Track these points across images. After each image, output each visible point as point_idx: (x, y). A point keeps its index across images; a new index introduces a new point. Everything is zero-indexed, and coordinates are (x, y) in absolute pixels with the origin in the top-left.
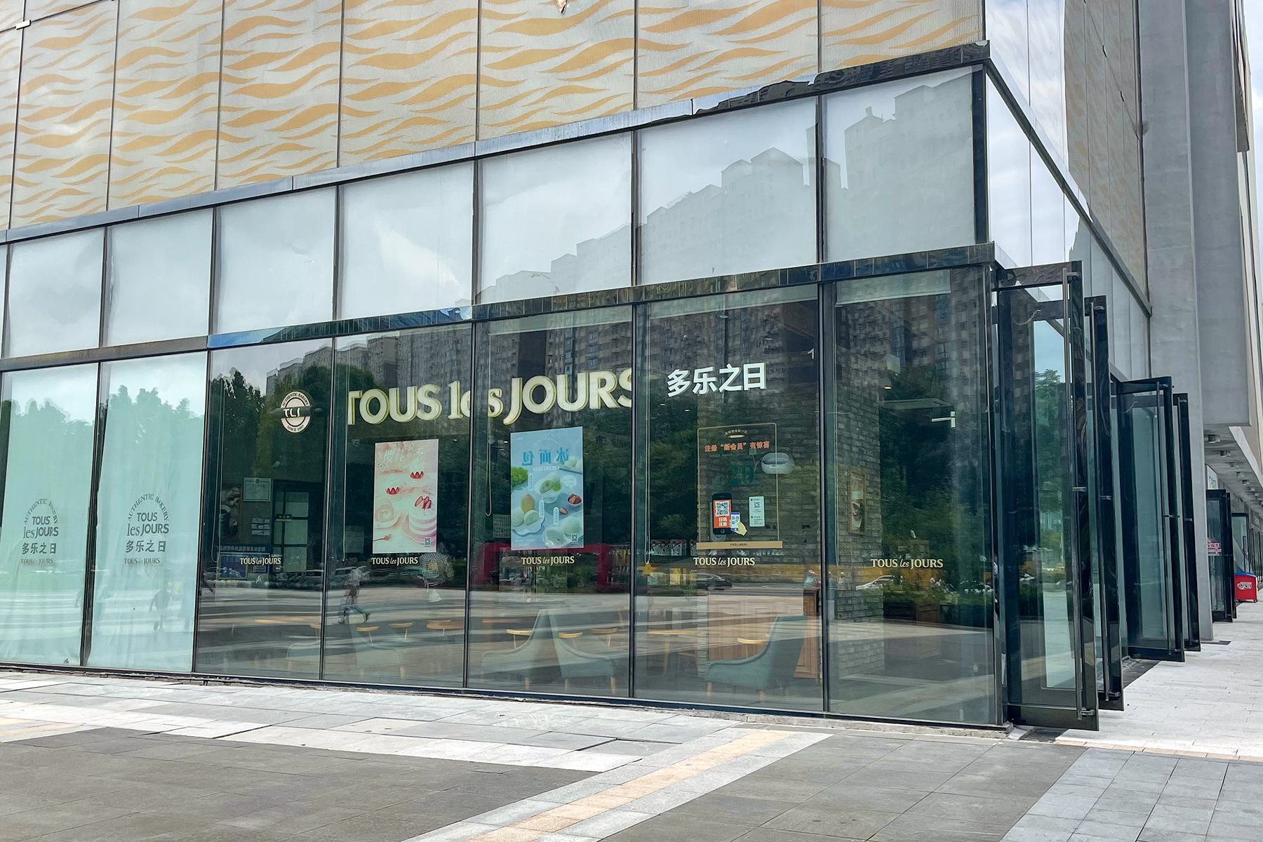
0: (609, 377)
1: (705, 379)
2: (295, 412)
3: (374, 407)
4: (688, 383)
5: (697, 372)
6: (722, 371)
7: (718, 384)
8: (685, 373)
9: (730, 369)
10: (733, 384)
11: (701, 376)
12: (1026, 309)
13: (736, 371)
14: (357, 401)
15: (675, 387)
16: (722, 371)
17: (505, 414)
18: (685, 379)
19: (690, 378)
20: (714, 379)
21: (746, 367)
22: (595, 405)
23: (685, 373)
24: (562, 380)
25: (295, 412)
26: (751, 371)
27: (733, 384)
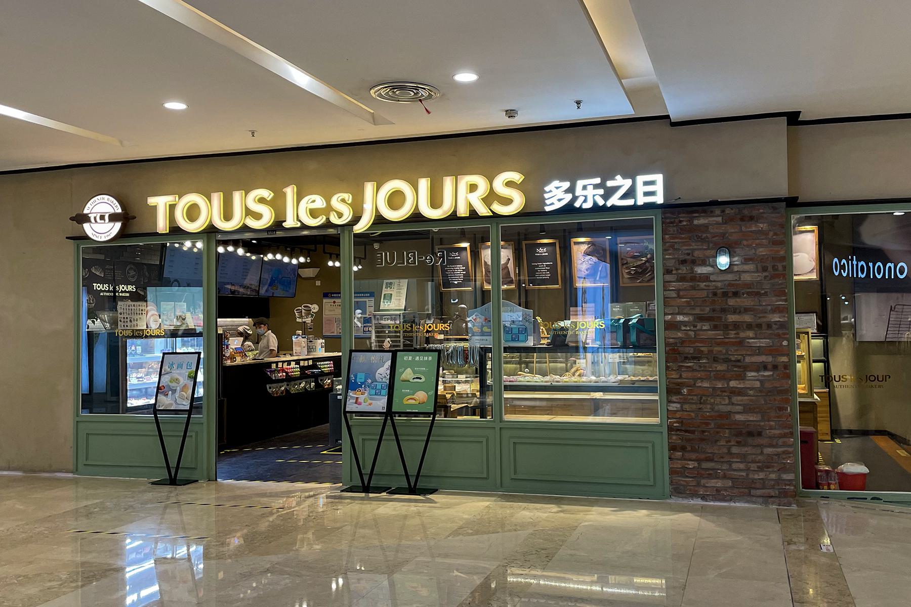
0: (480, 181)
1: (590, 192)
2: (102, 217)
3: (192, 213)
4: (569, 197)
5: (580, 183)
6: (610, 184)
7: (606, 197)
8: (567, 185)
9: (619, 181)
10: (625, 196)
11: (585, 188)
12: (309, 367)
13: (628, 183)
14: (172, 207)
15: (554, 200)
16: (610, 184)
17: (356, 219)
18: (567, 191)
19: (571, 190)
20: (601, 192)
21: (640, 179)
22: (463, 212)
23: (567, 185)
24: (424, 184)
25: (102, 217)
26: (646, 183)
27: (625, 196)
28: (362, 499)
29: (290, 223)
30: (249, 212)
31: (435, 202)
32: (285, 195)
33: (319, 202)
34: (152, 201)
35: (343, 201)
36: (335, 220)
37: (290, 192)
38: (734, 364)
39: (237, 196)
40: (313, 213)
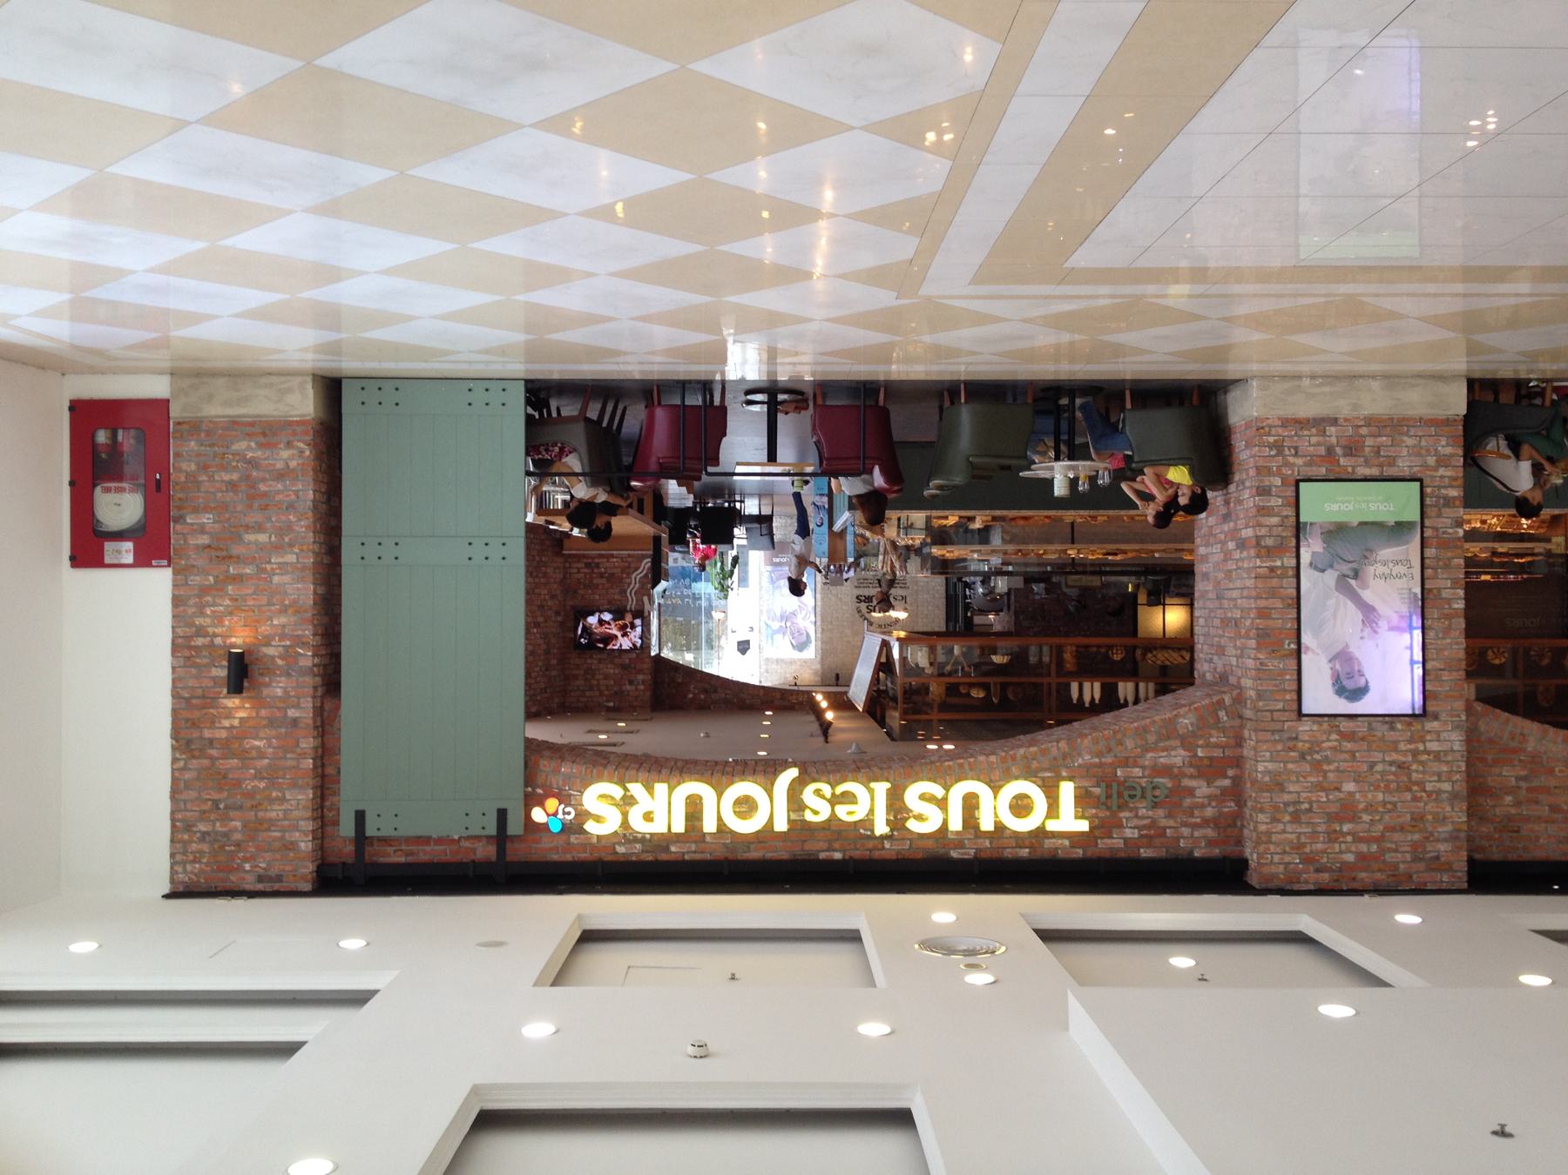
0: (639, 826)
14: (1053, 811)
24: (709, 826)
28: (426, 840)
29: (881, 788)
30: (942, 804)
31: (970, 803)
32: (888, 822)
33: (842, 812)
34: (1083, 826)
35: (816, 813)
36: (826, 789)
37: (881, 828)
38: (248, 429)
39: (956, 825)
40: (848, 798)
